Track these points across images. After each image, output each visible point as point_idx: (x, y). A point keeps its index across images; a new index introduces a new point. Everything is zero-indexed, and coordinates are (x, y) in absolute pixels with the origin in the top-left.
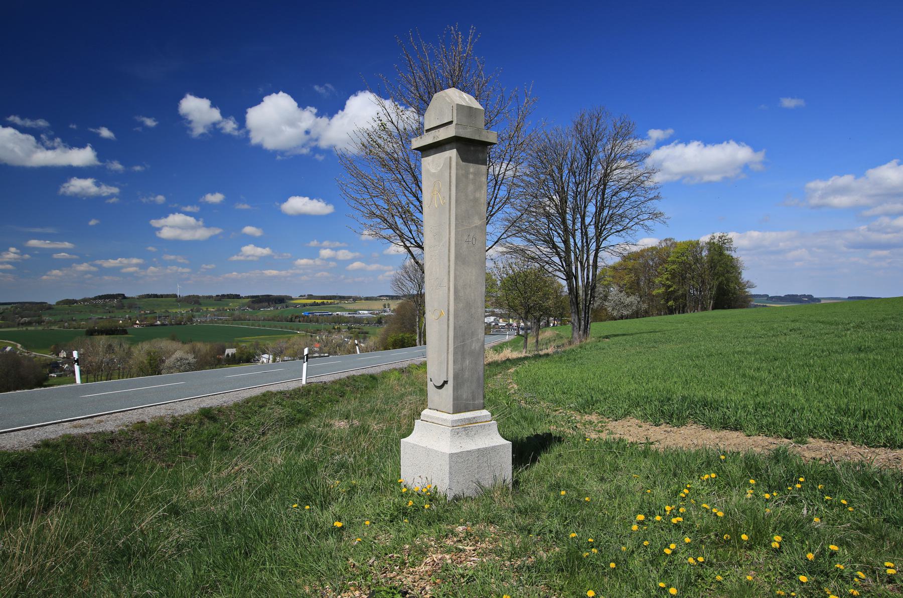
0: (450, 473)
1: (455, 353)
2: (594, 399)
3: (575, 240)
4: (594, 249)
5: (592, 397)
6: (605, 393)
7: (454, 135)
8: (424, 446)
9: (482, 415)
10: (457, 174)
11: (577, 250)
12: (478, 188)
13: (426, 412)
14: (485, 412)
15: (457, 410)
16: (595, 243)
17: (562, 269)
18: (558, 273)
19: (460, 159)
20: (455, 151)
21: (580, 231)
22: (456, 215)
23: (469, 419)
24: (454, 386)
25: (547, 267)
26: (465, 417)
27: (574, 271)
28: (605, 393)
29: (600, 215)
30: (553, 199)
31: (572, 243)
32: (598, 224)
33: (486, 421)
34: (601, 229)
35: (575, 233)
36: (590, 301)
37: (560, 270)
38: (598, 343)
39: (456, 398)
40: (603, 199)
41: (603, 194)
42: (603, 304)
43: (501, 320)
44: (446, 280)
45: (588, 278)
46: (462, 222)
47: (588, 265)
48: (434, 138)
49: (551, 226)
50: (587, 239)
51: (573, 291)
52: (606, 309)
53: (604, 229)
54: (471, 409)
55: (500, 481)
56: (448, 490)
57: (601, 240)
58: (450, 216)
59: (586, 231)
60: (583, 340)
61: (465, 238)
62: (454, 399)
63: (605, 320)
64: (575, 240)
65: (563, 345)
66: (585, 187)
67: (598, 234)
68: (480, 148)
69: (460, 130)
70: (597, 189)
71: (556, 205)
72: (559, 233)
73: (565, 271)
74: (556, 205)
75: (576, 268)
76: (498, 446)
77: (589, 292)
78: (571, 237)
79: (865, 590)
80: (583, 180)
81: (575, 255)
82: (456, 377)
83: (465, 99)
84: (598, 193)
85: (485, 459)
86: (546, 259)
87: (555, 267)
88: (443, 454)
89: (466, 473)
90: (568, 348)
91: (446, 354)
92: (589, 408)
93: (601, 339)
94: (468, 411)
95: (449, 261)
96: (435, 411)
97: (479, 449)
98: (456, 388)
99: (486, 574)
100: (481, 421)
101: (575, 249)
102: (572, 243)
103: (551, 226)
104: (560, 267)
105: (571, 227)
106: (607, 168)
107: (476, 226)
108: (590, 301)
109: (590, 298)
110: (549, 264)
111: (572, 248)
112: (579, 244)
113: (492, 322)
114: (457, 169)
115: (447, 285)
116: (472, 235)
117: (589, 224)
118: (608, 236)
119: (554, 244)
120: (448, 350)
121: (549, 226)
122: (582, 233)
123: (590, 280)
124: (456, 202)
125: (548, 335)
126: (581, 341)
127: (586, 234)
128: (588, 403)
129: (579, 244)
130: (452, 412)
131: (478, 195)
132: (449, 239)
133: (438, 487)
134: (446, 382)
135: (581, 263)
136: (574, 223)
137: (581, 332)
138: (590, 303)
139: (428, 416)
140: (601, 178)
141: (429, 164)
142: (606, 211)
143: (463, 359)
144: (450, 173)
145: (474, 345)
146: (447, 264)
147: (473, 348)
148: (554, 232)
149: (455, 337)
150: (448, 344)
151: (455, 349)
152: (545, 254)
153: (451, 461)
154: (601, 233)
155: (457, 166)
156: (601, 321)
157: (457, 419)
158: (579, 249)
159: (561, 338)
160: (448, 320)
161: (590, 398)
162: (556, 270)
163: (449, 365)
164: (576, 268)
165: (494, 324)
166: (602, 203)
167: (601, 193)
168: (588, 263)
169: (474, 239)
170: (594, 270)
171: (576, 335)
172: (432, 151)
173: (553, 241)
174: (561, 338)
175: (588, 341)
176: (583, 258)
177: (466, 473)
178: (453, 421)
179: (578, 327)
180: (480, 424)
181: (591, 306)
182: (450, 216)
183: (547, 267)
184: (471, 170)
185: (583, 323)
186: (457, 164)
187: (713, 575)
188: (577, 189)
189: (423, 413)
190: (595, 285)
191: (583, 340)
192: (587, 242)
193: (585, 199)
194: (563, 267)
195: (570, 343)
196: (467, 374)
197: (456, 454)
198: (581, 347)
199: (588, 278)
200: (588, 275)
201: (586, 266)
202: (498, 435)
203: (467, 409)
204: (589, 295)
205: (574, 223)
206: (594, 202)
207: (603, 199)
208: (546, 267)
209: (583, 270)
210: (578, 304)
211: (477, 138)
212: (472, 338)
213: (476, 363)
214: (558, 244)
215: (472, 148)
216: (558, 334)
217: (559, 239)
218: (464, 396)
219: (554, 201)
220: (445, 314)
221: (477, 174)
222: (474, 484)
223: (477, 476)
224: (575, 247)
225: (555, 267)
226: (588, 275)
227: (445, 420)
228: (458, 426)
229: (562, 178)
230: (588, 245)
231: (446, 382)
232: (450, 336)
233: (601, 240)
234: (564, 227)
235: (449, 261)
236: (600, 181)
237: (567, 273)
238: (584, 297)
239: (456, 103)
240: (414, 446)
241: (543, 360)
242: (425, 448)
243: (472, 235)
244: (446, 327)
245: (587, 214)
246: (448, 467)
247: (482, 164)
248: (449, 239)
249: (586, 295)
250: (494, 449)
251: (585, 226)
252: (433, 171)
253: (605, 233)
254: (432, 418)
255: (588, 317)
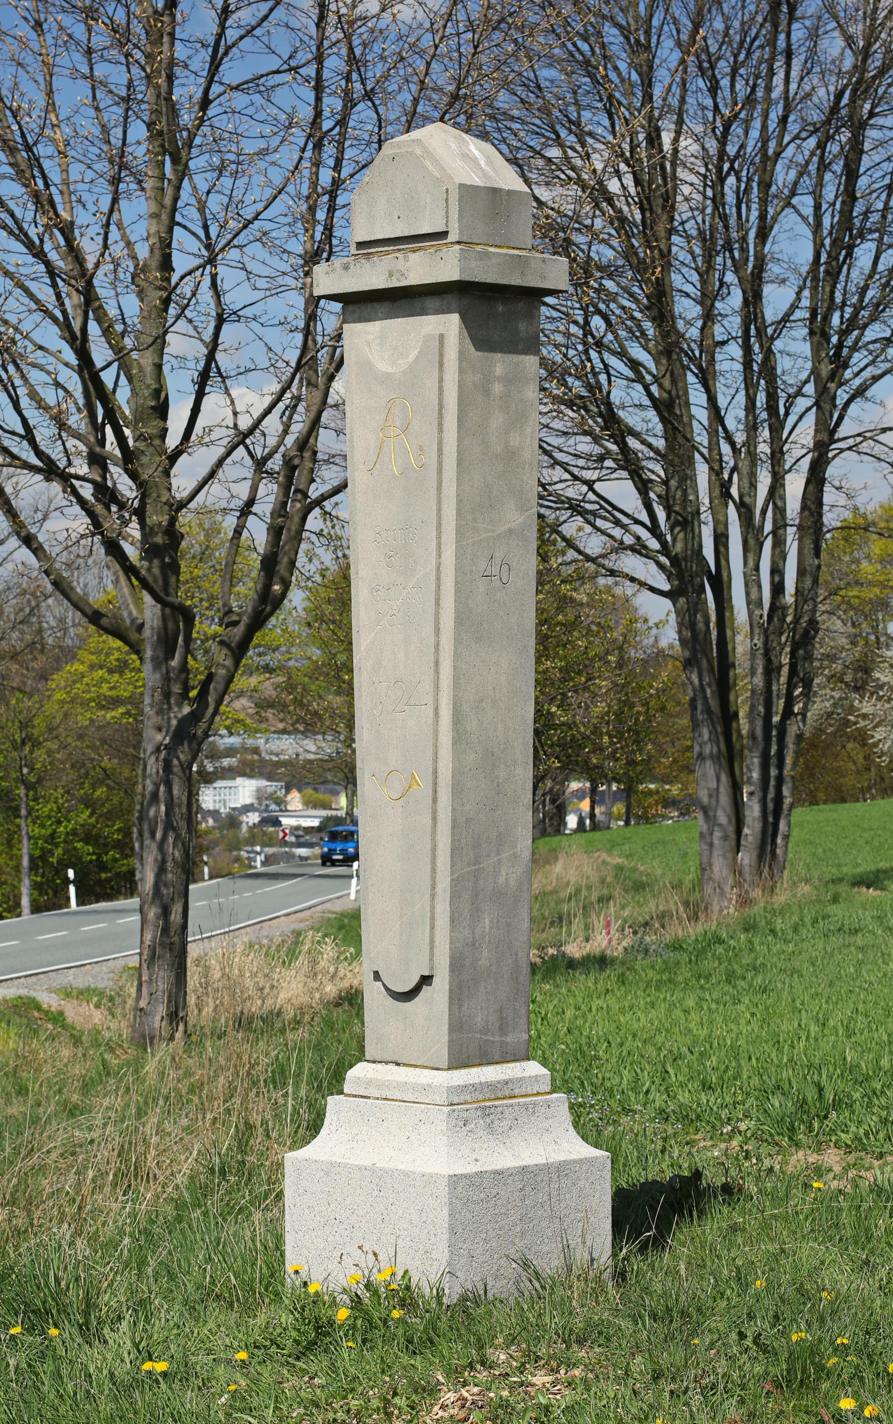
0: (453, 1231)
1: (455, 896)
2: (829, 1096)
3: (712, 400)
4: (809, 441)
5: (821, 1090)
6: (867, 1078)
7: (455, 277)
8: (368, 1163)
9: (527, 1074)
10: (461, 386)
11: (725, 448)
12: (516, 421)
13: (358, 1073)
14: (533, 1068)
15: (458, 1062)
16: (811, 417)
17: (654, 544)
18: (632, 564)
19: (468, 341)
20: (454, 319)
21: (735, 350)
22: (459, 502)
23: (491, 1086)
24: (451, 991)
25: (572, 527)
26: (483, 1080)
27: (709, 552)
28: (867, 1078)
29: (833, 275)
30: (604, 190)
31: (701, 414)
32: (826, 318)
33: (538, 1094)
34: (840, 346)
35: (712, 361)
36: (790, 701)
37: (639, 549)
38: (831, 909)
39: (457, 1026)
40: (850, 195)
41: (851, 174)
42: (851, 709)
43: (295, 800)
44: (427, 684)
45: (778, 589)
46: (475, 520)
47: (780, 525)
48: (391, 275)
49: (597, 322)
50: (772, 397)
51: (706, 653)
52: (862, 737)
53: (854, 348)
54: (497, 1058)
55: (581, 1256)
56: (447, 1278)
57: (842, 396)
58: (439, 502)
59: (768, 353)
60: (757, 893)
61: (482, 564)
62: (452, 1029)
63: (860, 795)
64: (712, 400)
65: (663, 917)
66: (764, 140)
67: (826, 369)
68: (521, 305)
69: (473, 264)
70: (822, 146)
71: (621, 221)
72: (634, 365)
73: (665, 549)
74: (621, 221)
75: (721, 539)
76: (574, 1162)
77: (785, 660)
78: (691, 378)
79: (141, 2)
80: (750, 100)
81: (716, 471)
82: (456, 965)
83: (475, 161)
84: (823, 167)
85: (542, 1197)
86: (571, 493)
87: (617, 532)
88: (430, 1179)
89: (491, 1234)
90: (693, 931)
91: (427, 898)
92: (810, 1129)
93: (843, 889)
94: (490, 1063)
95: (437, 630)
96: (391, 1066)
97: (524, 1168)
98: (457, 996)
99: (604, 1402)
100: (523, 1091)
101: (713, 445)
102: (701, 414)
103: (597, 322)
104: (644, 534)
105: (694, 333)
106: (868, 45)
107: (510, 531)
108: (790, 701)
109: (791, 687)
110: (583, 513)
111: (701, 438)
112: (734, 418)
113: (248, 809)
114: (461, 371)
115: (430, 701)
116: (499, 555)
117: (786, 319)
118: (876, 379)
119: (610, 418)
120: (433, 887)
121: (586, 326)
122: (747, 363)
123: (789, 597)
124: (459, 465)
125: (572, 876)
126: (745, 901)
127: (769, 370)
128: (807, 1112)
129: (734, 418)
130: (445, 1065)
131: (514, 440)
132: (438, 569)
133: (411, 1273)
134: (426, 980)
135: (745, 510)
136: (709, 317)
137: (746, 858)
138: (788, 712)
139: (369, 1083)
140: (839, 96)
141: (369, 344)
142: (864, 253)
143: (476, 913)
144: (441, 380)
145: (503, 872)
146: (432, 640)
147: (501, 880)
148: (614, 362)
149: (455, 850)
150: (434, 870)
151: (455, 882)
152: (564, 466)
153: (452, 1195)
154: (840, 362)
155: (461, 361)
156: (841, 798)
157: (462, 1083)
158: (732, 444)
159: (639, 887)
160: (435, 800)
161: (811, 1094)
162: (621, 547)
163: (438, 928)
164: (721, 539)
165: (253, 818)
166: (846, 215)
167: (838, 167)
168: (780, 511)
169: (505, 567)
170: (809, 544)
171: (719, 868)
172: (380, 308)
173: (609, 404)
174: (639, 887)
175: (781, 898)
176: (753, 486)
177: (491, 1234)
178: (451, 1090)
179: (731, 829)
180: (522, 1100)
181: (793, 729)
182: (439, 502)
183: (572, 527)
184: (499, 370)
185: (753, 811)
186: (462, 356)
187: (848, 678)
188: (723, 141)
189: (351, 1074)
190: (813, 624)
191: (757, 893)
192: (771, 408)
193: (764, 202)
194: (654, 529)
195: (695, 910)
196: (485, 957)
197: (465, 1176)
198: (749, 927)
199: (778, 589)
200: (777, 571)
201: (768, 527)
202: (572, 1132)
203: (485, 1060)
204: (785, 671)
205: (709, 317)
206: (808, 211)
207: (850, 195)
208: (569, 530)
209: (751, 546)
210: (728, 717)
211: (516, 280)
212: (498, 854)
213: (509, 925)
214: (631, 418)
215: (501, 308)
216: (620, 868)
217: (638, 393)
218: (479, 1020)
219: (610, 201)
220: (423, 786)
221: (512, 380)
222: (514, 1265)
223: (520, 1244)
224: (712, 434)
225: (617, 532)
226: (777, 571)
227: (425, 1088)
228: (466, 1103)
229: (648, 83)
230: (777, 426)
231: (426, 980)
232: (440, 846)
233: (842, 396)
234: (665, 335)
235: (437, 630)
236: (835, 109)
237: (675, 561)
238: (759, 680)
239: (458, 181)
240: (330, 1169)
241: (584, 982)
242: (372, 1170)
243: (499, 555)
244: (428, 821)
245: (773, 269)
246: (446, 1212)
247: (525, 352)
248: (438, 569)
249: (771, 671)
250: (562, 1169)
251: (760, 332)
252: (384, 367)
253: (859, 359)
254: (380, 1085)
255: (780, 780)
